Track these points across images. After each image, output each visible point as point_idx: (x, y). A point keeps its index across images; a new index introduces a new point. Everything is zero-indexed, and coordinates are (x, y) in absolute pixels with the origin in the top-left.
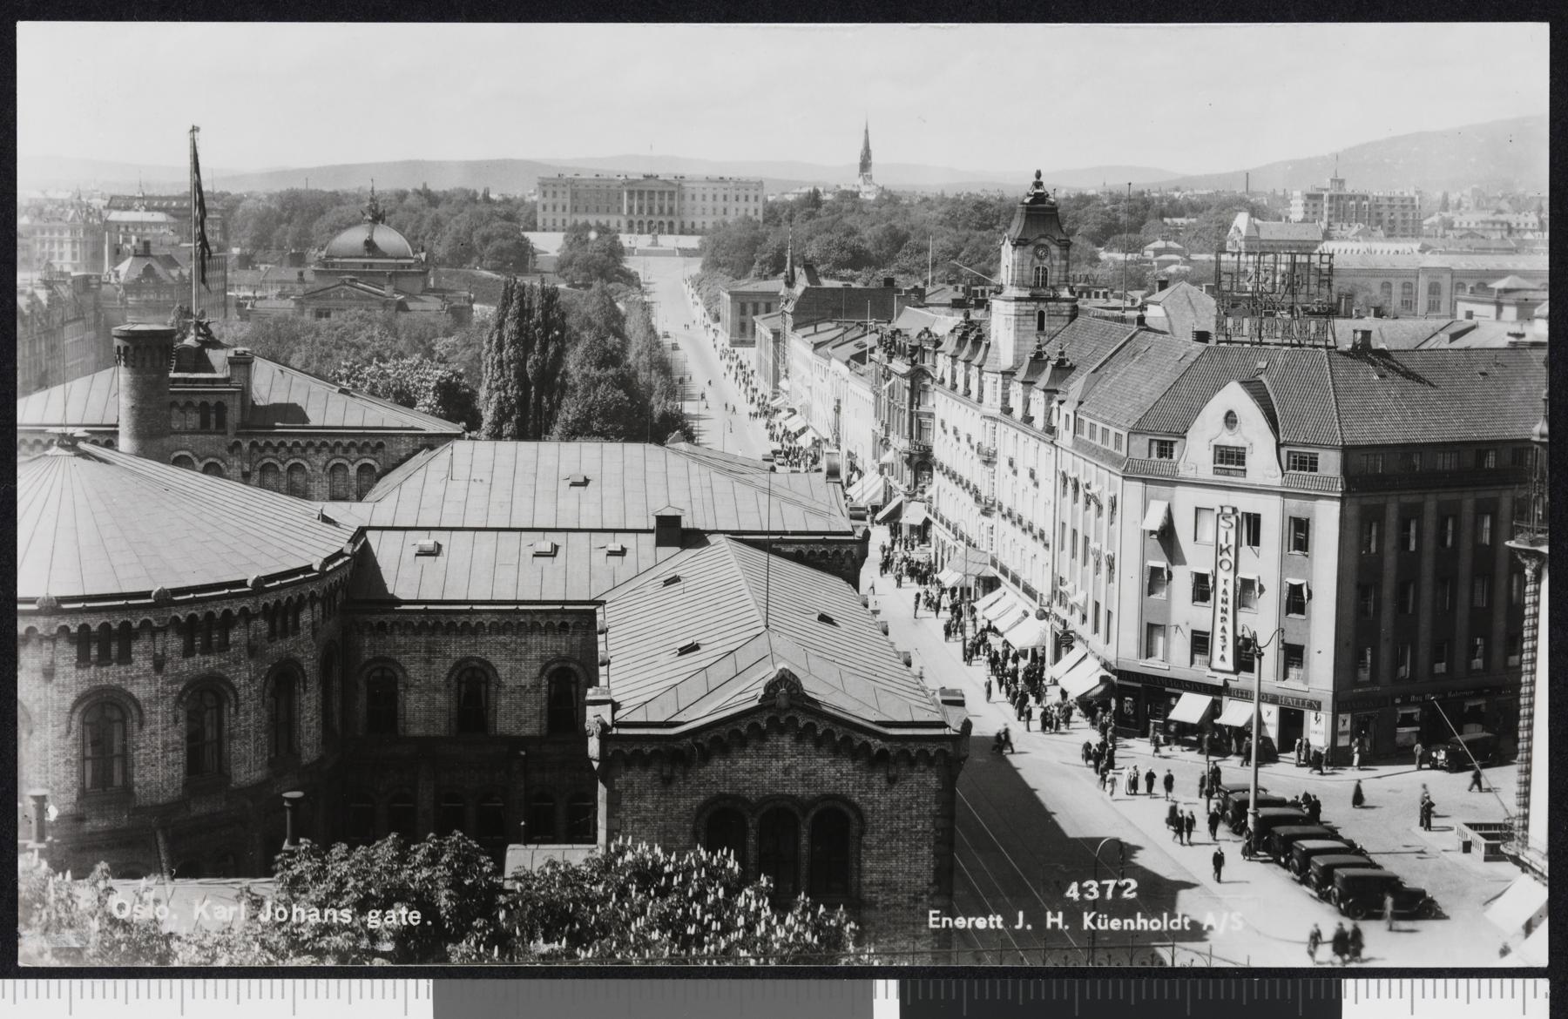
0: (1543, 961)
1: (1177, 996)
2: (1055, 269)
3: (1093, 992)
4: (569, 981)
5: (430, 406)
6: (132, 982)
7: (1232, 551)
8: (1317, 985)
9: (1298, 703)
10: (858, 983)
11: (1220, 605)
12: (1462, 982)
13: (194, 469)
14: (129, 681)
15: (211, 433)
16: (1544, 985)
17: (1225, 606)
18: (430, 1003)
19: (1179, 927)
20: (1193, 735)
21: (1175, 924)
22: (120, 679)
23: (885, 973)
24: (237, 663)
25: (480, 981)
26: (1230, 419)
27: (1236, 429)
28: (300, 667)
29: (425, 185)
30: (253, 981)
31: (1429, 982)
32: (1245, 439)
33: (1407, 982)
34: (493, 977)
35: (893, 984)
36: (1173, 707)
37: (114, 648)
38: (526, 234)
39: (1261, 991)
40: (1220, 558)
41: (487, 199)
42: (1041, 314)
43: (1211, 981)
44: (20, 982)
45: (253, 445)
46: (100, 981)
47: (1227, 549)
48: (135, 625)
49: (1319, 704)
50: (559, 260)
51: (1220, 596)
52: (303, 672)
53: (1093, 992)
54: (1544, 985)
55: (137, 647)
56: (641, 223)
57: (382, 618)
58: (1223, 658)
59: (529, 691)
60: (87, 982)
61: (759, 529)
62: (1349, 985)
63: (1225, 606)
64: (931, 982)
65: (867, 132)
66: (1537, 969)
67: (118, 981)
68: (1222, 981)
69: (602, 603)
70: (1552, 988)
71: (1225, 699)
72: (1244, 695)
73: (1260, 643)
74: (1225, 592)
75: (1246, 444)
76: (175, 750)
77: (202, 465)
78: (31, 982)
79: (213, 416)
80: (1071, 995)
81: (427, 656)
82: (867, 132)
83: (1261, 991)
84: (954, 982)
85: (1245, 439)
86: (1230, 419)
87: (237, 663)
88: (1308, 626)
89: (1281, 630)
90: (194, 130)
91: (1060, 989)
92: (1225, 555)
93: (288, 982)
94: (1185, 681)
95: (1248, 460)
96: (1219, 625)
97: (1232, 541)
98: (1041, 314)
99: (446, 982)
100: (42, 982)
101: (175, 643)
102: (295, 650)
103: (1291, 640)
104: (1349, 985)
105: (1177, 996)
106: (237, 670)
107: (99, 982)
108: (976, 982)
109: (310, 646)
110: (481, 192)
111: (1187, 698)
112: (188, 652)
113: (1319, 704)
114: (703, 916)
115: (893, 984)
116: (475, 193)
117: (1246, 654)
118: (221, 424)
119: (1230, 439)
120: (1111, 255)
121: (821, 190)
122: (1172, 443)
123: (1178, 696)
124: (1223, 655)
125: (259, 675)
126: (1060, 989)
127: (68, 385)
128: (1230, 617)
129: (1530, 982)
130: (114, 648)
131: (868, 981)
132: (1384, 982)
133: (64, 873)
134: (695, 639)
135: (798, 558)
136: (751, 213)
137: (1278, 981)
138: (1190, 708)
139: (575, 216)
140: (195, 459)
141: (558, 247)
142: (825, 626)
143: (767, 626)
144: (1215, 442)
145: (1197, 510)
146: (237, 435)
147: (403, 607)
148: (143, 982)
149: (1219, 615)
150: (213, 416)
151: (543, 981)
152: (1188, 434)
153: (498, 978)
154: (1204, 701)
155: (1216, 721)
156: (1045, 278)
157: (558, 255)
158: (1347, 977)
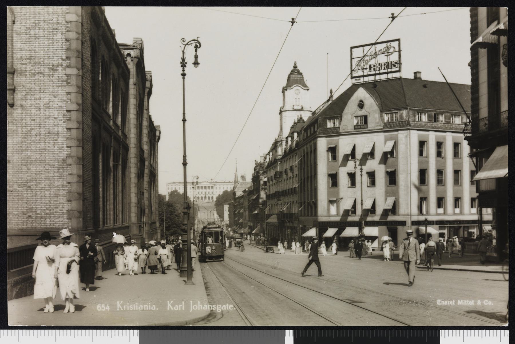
3: (321, 334)
4: (184, 331)
6: (39, 331)
16: (507, 332)
19: (177, 309)
20: (255, 210)
21: (205, 308)
23: (289, 328)
25: (154, 331)
26: (361, 105)
30: (79, 330)
31: (469, 331)
33: (462, 331)
34: (159, 329)
35: (291, 332)
39: (413, 335)
44: (9, 331)
46: (125, 331)
53: (321, 334)
54: (507, 332)
62: (442, 332)
64: (356, 331)
78: (13, 331)
80: (313, 335)
83: (413, 335)
84: (311, 331)
86: (361, 105)
91: (380, 333)
93: (54, 331)
99: (143, 331)
100: (106, 331)
104: (442, 332)
114: (123, 308)
115: (291, 332)
126: (380, 333)
132: (491, 331)
133: (452, 301)
135: (374, 145)
137: (419, 331)
145: (398, 40)
147: (152, 183)
148: (43, 331)
151: (176, 330)
153: (160, 329)
155: (237, 196)
158: (442, 329)
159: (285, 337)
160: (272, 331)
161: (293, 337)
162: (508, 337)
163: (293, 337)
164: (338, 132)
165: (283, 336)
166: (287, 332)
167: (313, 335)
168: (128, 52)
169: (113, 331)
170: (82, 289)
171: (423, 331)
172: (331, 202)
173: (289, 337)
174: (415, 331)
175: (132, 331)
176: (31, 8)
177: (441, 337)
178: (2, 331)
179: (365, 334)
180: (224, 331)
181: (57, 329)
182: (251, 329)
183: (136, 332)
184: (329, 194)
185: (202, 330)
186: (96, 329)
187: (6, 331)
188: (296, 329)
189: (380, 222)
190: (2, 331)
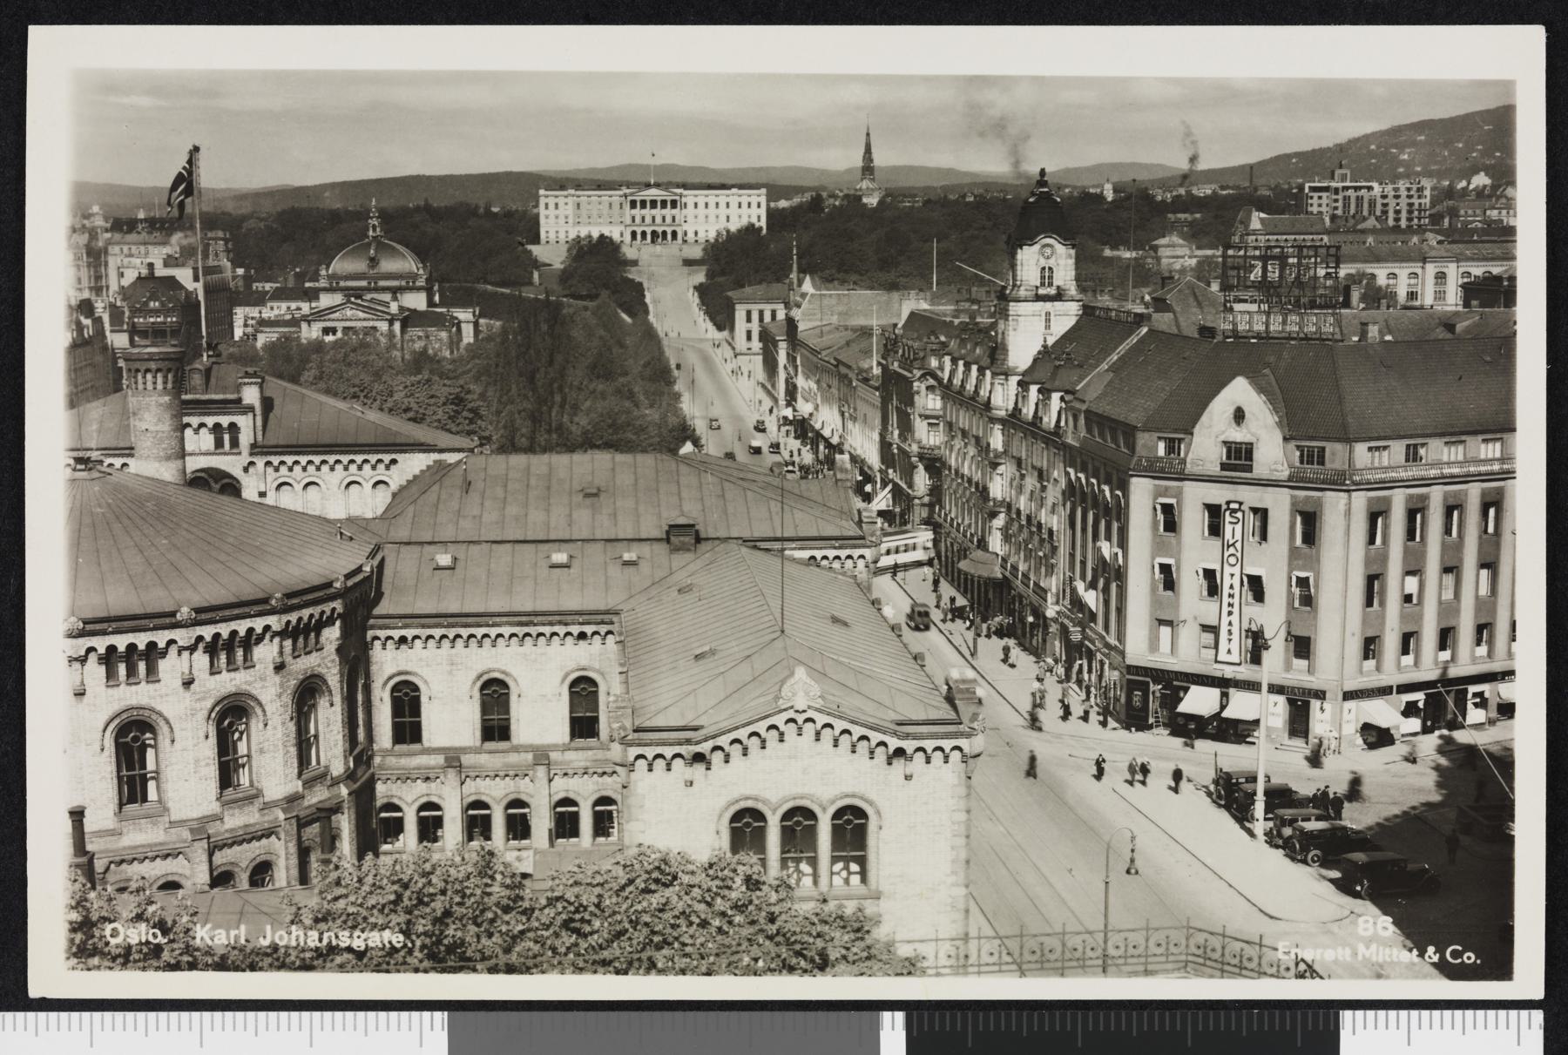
0: (1538, 993)
1: (1178, 1028)
2: (1061, 268)
3: (1096, 1023)
5: (439, 421)
7: (1238, 545)
8: (1316, 1016)
9: (1304, 693)
10: (866, 1014)
11: (1226, 600)
12: (1458, 1013)
13: (210, 489)
14: (158, 699)
15: (225, 454)
16: (1538, 1016)
17: (1231, 600)
18: (444, 1035)
22: (150, 698)
24: (263, 679)
26: (1239, 416)
27: (1243, 425)
28: (325, 682)
29: (426, 200)
30: (271, 1013)
32: (1253, 435)
35: (900, 1016)
36: (1181, 699)
37: (142, 666)
38: (529, 247)
39: (1261, 1022)
40: (1226, 554)
41: (488, 213)
42: (1048, 314)
43: (1211, 1013)
45: (268, 463)
47: (1233, 545)
48: (162, 645)
49: (1324, 693)
50: (564, 271)
51: (1226, 591)
52: (328, 687)
53: (1096, 1023)
55: (163, 665)
56: (644, 234)
57: (403, 632)
58: (1229, 652)
59: (550, 701)
60: (108, 1015)
61: (772, 535)
62: (1346, 1016)
63: (1231, 600)
64: (937, 1014)
65: (868, 134)
66: (1531, 1002)
67: (139, 1014)
68: (1222, 1013)
69: (617, 613)
70: (1546, 1020)
71: (1232, 691)
72: (1253, 686)
73: (1267, 635)
74: (1231, 587)
75: (1252, 439)
76: (208, 765)
77: (217, 487)
79: (226, 437)
80: (1184, 1023)
81: (449, 668)
82: (868, 134)
83: (1261, 1022)
85: (1253, 435)
86: (1239, 416)
87: (263, 679)
88: (1315, 618)
89: (1289, 623)
90: (196, 149)
92: (1232, 550)
94: (1193, 675)
95: (1256, 455)
96: (1225, 620)
97: (1238, 536)
98: (1048, 314)
99: (459, 1015)
101: (201, 659)
102: (319, 665)
103: (1300, 631)
104: (1346, 1016)
105: (1178, 1028)
106: (263, 687)
107: (119, 1015)
108: (981, 1014)
109: (333, 661)
110: (482, 204)
111: (1195, 691)
112: (214, 671)
113: (1324, 693)
115: (900, 1016)
116: (477, 207)
117: (1257, 645)
118: (235, 443)
119: (1238, 435)
120: (1116, 253)
121: (824, 194)
122: (1180, 440)
123: (1186, 690)
124: (1233, 648)
125: (285, 691)
127: (81, 408)
128: (1236, 610)
129: (1524, 1013)
130: (142, 666)
131: (875, 1013)
132: (1381, 1013)
134: (713, 645)
136: (754, 220)
138: (1199, 701)
139: (577, 228)
140: (210, 480)
141: (563, 259)
142: (837, 630)
143: (783, 632)
144: (1222, 438)
146: (251, 454)
149: (1225, 609)
150: (226, 437)
152: (1196, 430)
154: (1215, 693)
156: (1051, 277)
157: (562, 267)
159: (882, 1034)
160: (843, 1014)
161: (904, 1033)
162: (1541, 1032)
163: (904, 1034)
164: (1182, 471)
165: (875, 1029)
166: (886, 1016)
167: (1184, 1023)
168: (108, 643)
169: (371, 1015)
170: (1433, 764)
171: (1288, 1013)
172: (1409, 573)
173: (893, 1035)
174: (1266, 1013)
175: (426, 1014)
176: (655, 301)
177: (1342, 1031)
178: (9, 1015)
179: (953, 1024)
180: (745, 1015)
181: (206, 1010)
182: (780, 1010)
183: (440, 1017)
184: (1156, 603)
185: (514, 1013)
186: (892, 1010)
187: (20, 1015)
188: (910, 1008)
189: (1188, 682)
190: (9, 1016)
